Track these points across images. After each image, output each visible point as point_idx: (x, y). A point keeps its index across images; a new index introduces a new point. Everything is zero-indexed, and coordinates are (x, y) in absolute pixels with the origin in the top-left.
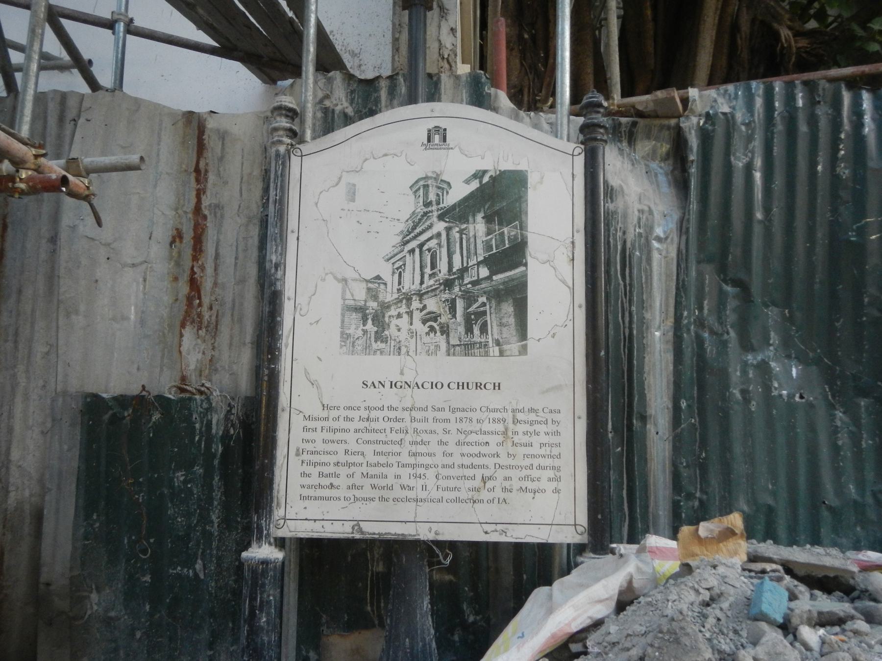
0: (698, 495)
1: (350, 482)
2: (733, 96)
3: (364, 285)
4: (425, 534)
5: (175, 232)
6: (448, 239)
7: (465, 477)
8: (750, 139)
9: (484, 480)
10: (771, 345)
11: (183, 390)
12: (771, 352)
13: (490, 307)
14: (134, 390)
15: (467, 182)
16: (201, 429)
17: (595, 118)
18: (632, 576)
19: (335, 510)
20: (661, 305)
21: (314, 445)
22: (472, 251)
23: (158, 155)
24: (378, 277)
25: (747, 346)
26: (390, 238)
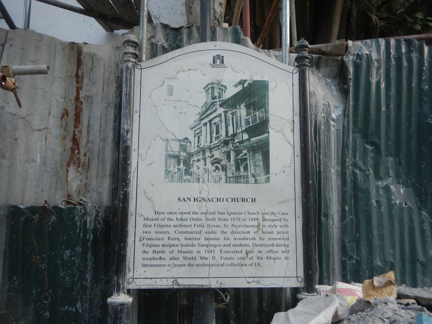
0: (355, 257)
1: (171, 255)
2: (370, 46)
3: (178, 143)
4: (214, 284)
5: (64, 111)
6: (225, 118)
7: (237, 252)
8: (378, 69)
9: (247, 253)
10: (390, 177)
11: (68, 203)
12: (390, 180)
13: (249, 156)
14: (41, 203)
15: (236, 86)
16: (80, 226)
17: (303, 54)
18: (338, 309)
19: (163, 272)
20: (335, 155)
21: (150, 235)
22: (239, 125)
23: (54, 67)
24: (186, 139)
25: (378, 177)
26: (193, 117)
